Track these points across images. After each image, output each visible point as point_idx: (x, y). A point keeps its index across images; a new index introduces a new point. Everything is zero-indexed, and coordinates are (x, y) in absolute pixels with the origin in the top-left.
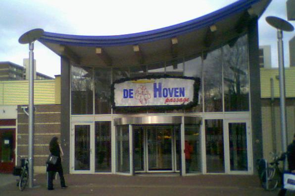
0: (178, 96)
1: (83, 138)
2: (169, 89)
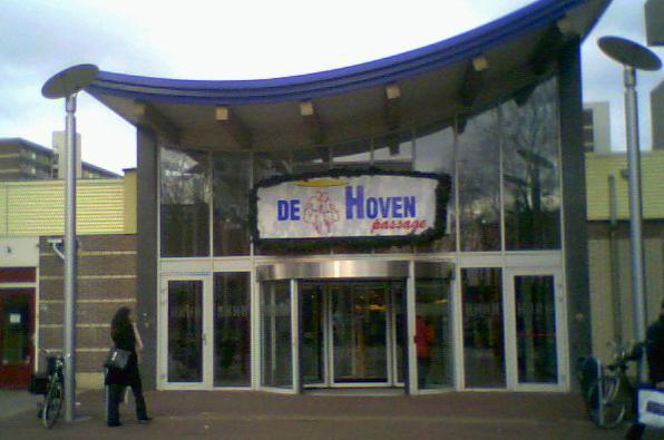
0: (400, 216)
1: (187, 310)
2: (381, 199)
